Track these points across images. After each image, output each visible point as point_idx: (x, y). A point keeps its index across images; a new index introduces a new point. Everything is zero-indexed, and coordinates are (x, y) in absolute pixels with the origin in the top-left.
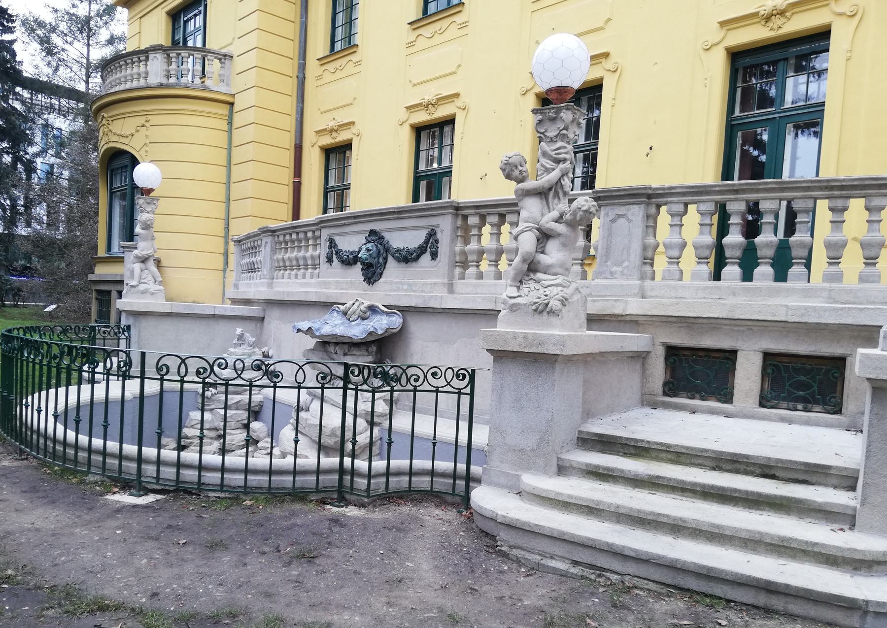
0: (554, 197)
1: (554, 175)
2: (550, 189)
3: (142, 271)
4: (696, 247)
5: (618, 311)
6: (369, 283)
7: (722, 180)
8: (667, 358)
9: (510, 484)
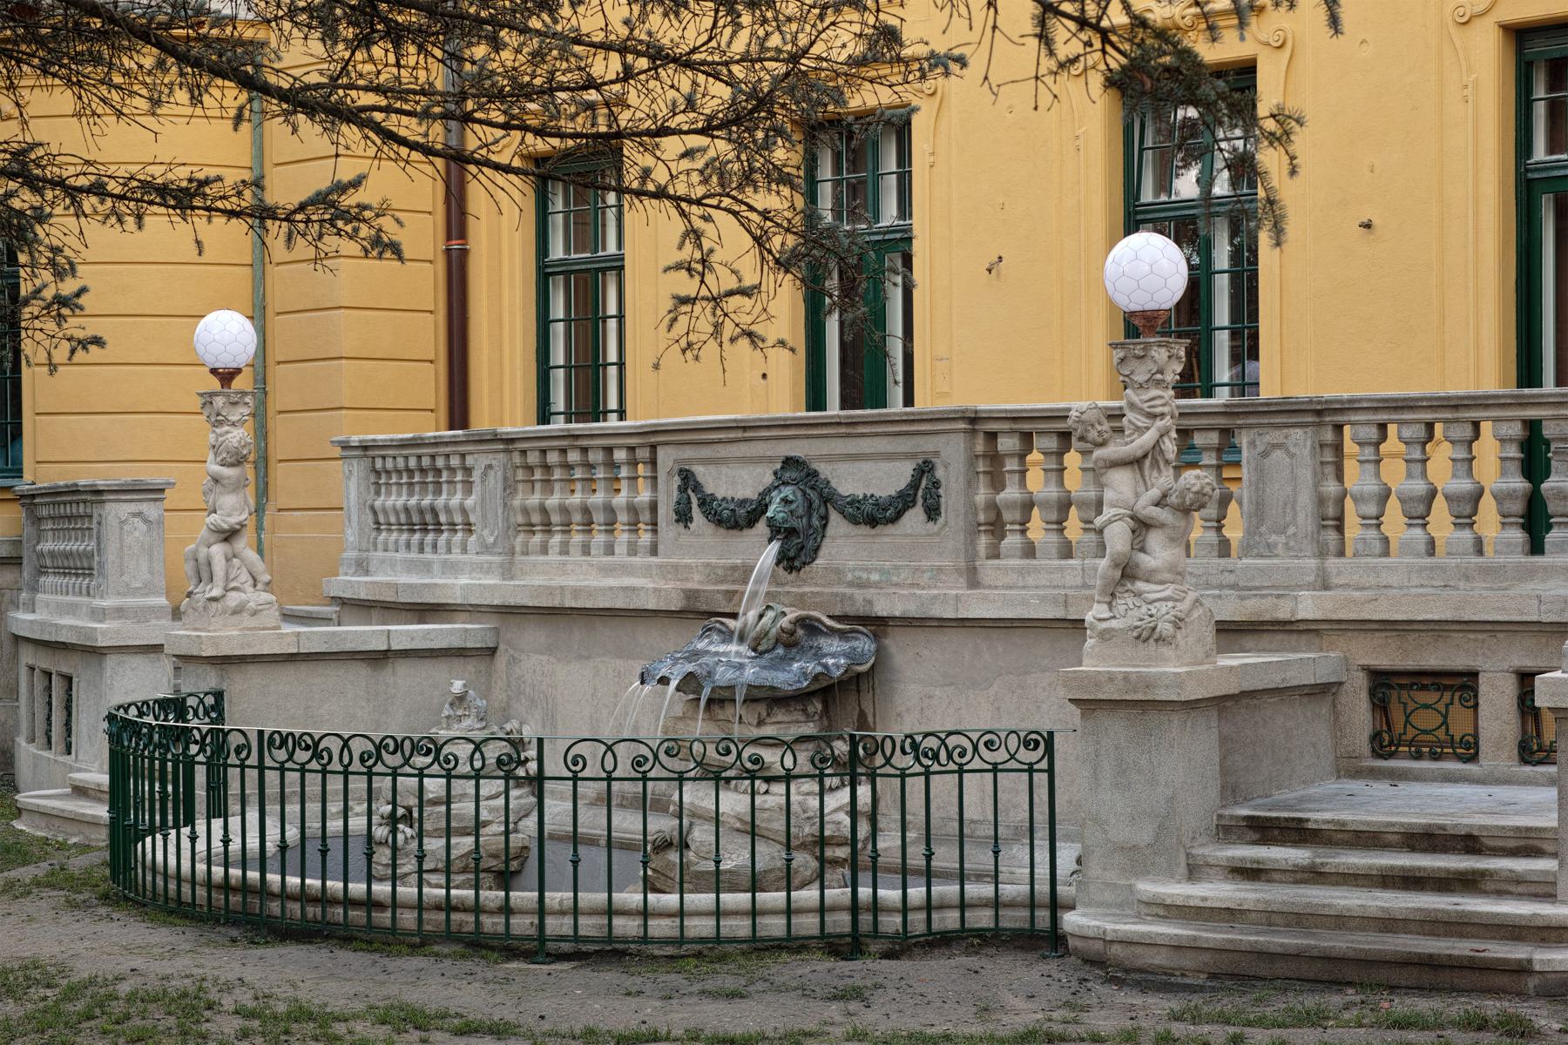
1: (1149, 438)
2: (1145, 456)
3: (228, 560)
5: (1283, 615)
6: (790, 569)
8: (1372, 693)
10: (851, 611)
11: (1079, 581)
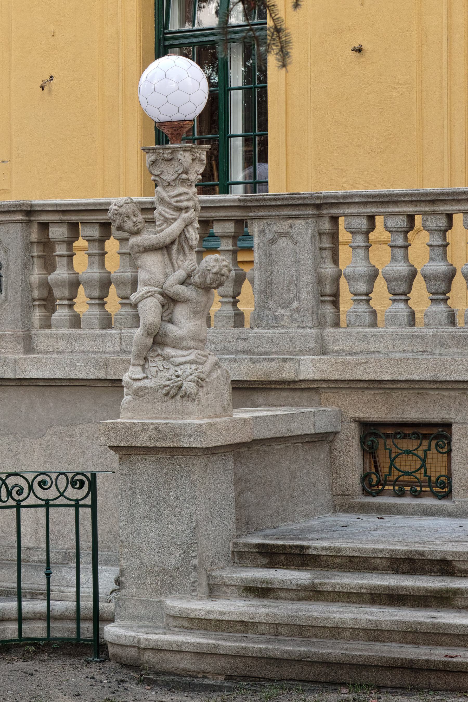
0: (179, 251)
2: (173, 243)
4: (388, 280)
5: (288, 375)
8: (363, 441)
11: (117, 347)
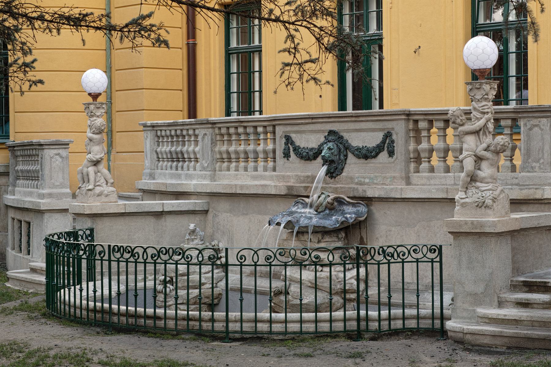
1: (482, 122)
2: (480, 130)
3: (95, 173)
5: (538, 196)
7: (339, 110)
9: (469, 316)
10: (357, 195)
11: (452, 182)
